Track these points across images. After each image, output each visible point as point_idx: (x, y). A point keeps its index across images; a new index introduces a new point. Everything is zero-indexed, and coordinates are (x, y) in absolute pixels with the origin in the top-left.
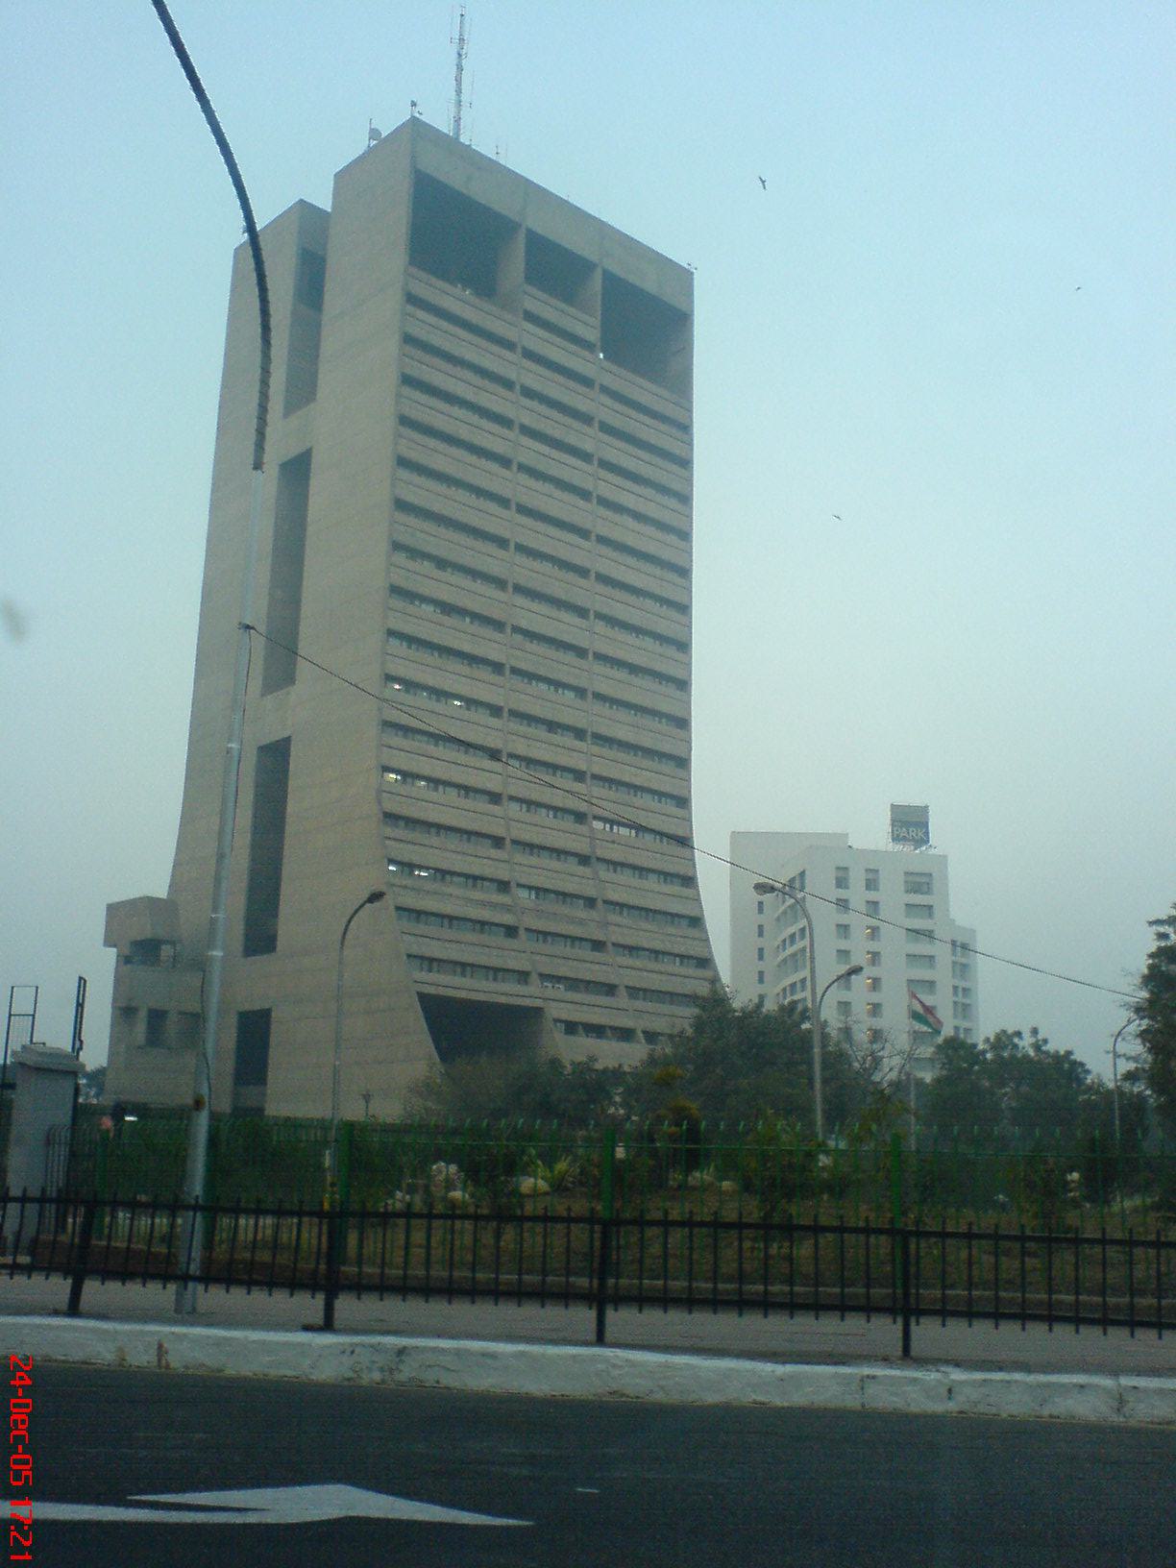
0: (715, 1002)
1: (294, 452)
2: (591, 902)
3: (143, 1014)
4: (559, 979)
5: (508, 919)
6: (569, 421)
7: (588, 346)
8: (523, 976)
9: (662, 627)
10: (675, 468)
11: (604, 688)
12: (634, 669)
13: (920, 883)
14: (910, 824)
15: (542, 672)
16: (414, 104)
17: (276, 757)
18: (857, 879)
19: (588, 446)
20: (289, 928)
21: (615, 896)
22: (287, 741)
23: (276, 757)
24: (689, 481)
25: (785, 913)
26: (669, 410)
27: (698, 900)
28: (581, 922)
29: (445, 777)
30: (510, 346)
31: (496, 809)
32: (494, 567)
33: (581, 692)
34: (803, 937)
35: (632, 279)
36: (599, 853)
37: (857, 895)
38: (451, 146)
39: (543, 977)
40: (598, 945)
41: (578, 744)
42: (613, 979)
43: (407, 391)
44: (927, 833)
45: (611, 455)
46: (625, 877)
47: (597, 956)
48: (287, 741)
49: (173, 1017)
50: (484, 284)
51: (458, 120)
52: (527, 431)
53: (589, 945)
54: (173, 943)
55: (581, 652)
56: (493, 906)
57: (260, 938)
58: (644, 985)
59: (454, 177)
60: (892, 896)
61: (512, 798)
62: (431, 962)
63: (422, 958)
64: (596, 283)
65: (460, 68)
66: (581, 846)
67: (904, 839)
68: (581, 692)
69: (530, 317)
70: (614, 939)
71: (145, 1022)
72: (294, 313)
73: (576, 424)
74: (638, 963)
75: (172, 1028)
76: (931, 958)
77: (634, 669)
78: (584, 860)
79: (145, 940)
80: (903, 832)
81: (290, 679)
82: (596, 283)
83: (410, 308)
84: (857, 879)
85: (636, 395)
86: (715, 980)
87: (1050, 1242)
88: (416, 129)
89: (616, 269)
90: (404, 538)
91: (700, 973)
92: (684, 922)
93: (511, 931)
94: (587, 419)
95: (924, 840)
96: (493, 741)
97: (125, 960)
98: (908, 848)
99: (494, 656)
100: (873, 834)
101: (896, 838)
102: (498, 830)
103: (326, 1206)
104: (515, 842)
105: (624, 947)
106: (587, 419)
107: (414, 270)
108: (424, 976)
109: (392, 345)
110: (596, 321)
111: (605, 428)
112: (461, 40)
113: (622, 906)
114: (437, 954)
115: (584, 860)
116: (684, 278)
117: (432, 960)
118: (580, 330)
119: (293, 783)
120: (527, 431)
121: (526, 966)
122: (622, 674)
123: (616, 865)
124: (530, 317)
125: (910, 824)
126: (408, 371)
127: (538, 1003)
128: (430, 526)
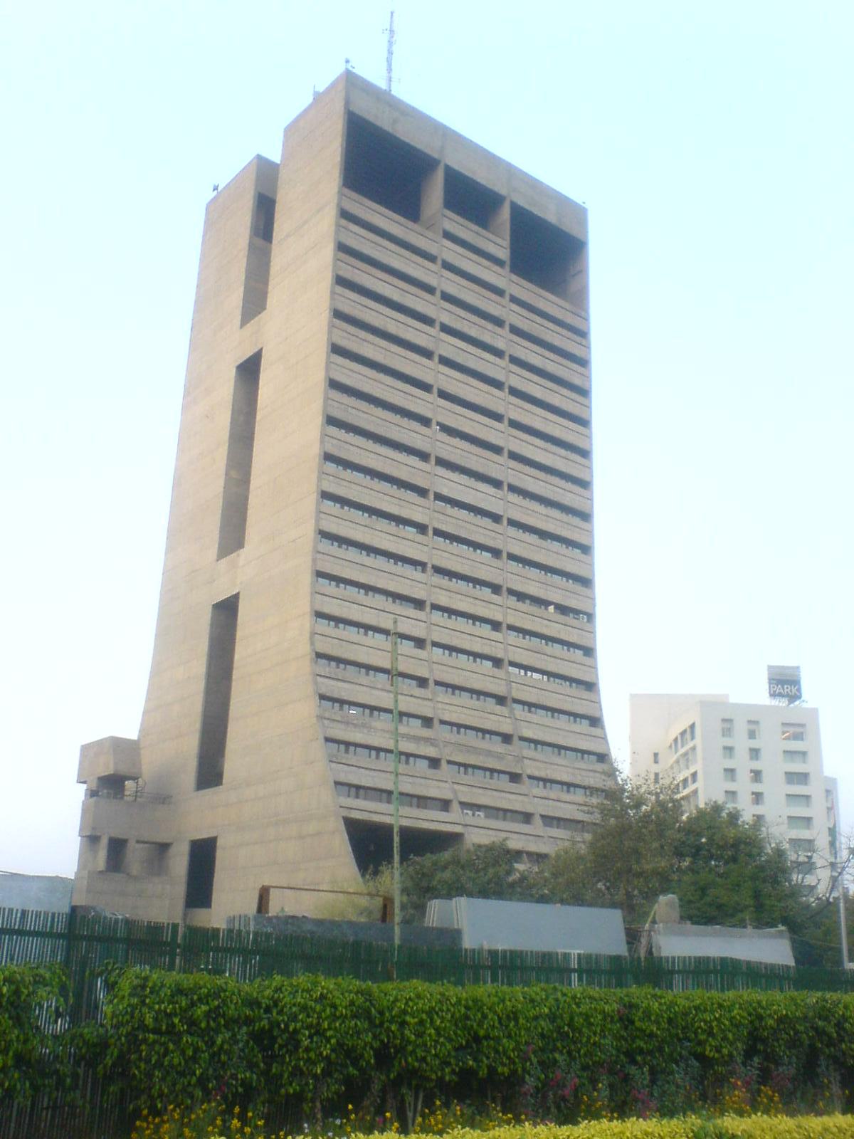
0: (614, 794)
1: (249, 354)
2: (507, 738)
3: (104, 842)
4: (479, 807)
5: (431, 752)
6: (483, 322)
7: (498, 262)
8: (445, 805)
9: (567, 500)
10: (574, 366)
11: (517, 550)
12: (544, 535)
13: (798, 731)
14: (785, 683)
15: (463, 534)
16: (347, 61)
17: (227, 611)
18: (741, 728)
19: (500, 344)
20: (234, 763)
21: (528, 733)
22: (236, 596)
23: (227, 611)
24: (588, 377)
25: (677, 762)
26: (570, 319)
27: (604, 738)
28: (499, 757)
29: (373, 623)
30: (431, 258)
31: (421, 654)
32: (419, 443)
33: (496, 553)
34: (694, 781)
35: (536, 211)
36: (515, 694)
37: (741, 743)
38: (384, 98)
39: (464, 805)
40: (515, 778)
41: (495, 598)
42: (529, 809)
43: (339, 289)
44: (799, 690)
45: (521, 354)
46: (540, 717)
47: (513, 787)
48: (236, 596)
49: (132, 845)
50: (409, 207)
51: (390, 80)
52: (446, 329)
53: (507, 777)
54: (135, 778)
55: (496, 518)
56: (417, 739)
57: (210, 772)
58: (557, 815)
59: (383, 120)
60: (772, 743)
61: (435, 644)
62: (359, 790)
63: (350, 785)
64: (505, 214)
65: (390, 53)
66: (500, 689)
67: (780, 695)
68: (496, 553)
69: (448, 235)
70: (529, 772)
71: (111, 850)
72: (251, 245)
73: (490, 326)
74: (552, 795)
75: (135, 856)
76: (808, 797)
77: (544, 535)
78: (501, 700)
79: (112, 778)
80: (779, 689)
81: (239, 544)
82: (505, 214)
83: (344, 222)
84: (741, 728)
85: (541, 305)
86: (612, 773)
87: (312, 944)
88: (351, 81)
89: (521, 202)
90: (338, 414)
91: (599, 767)
92: (594, 758)
93: (434, 763)
94: (498, 322)
95: (795, 697)
96: (418, 593)
97: (92, 793)
98: (783, 703)
99: (418, 517)
100: (756, 693)
101: (773, 695)
102: (422, 672)
103: (164, 1027)
104: (437, 683)
105: (538, 779)
106: (498, 322)
107: (346, 191)
108: (351, 802)
109: (328, 251)
110: (506, 243)
111: (515, 330)
112: (392, 31)
113: (536, 742)
114: (364, 783)
115: (501, 700)
116: (580, 214)
117: (358, 788)
118: (491, 249)
119: (240, 634)
120: (446, 329)
121: (447, 795)
122: (533, 539)
123: (531, 706)
124: (448, 235)
125: (785, 683)
126: (341, 273)
127: (458, 829)
128: (363, 405)
